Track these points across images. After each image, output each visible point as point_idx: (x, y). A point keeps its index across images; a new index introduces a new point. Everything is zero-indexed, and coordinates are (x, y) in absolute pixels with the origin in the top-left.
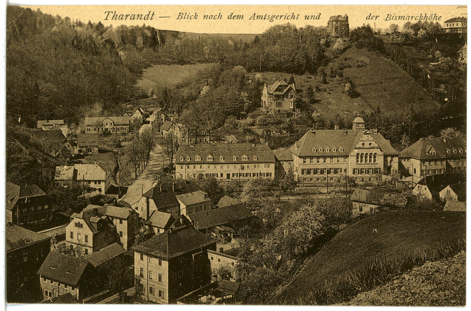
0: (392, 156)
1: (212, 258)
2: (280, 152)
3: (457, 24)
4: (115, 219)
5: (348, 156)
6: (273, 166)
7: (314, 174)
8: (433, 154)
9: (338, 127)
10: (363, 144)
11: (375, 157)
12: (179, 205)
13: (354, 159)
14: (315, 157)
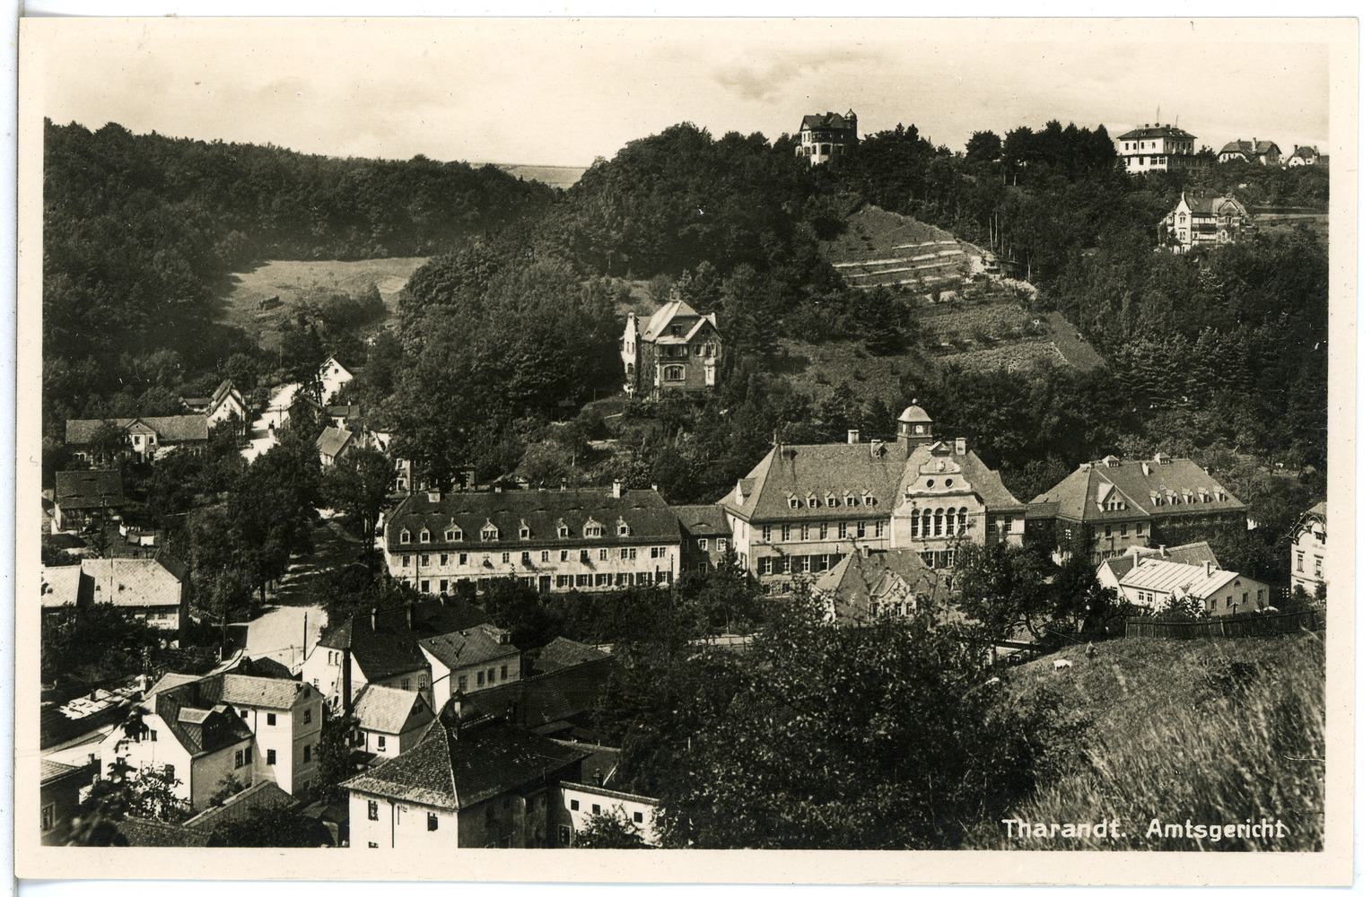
0: (1009, 516)
1: (575, 805)
2: (692, 514)
3: (1154, 144)
4: (251, 714)
5: (889, 518)
6: (674, 551)
7: (773, 573)
8: (1116, 508)
9: (857, 436)
10: (930, 483)
11: (962, 518)
12: (429, 668)
13: (907, 526)
14: (870, 518)
